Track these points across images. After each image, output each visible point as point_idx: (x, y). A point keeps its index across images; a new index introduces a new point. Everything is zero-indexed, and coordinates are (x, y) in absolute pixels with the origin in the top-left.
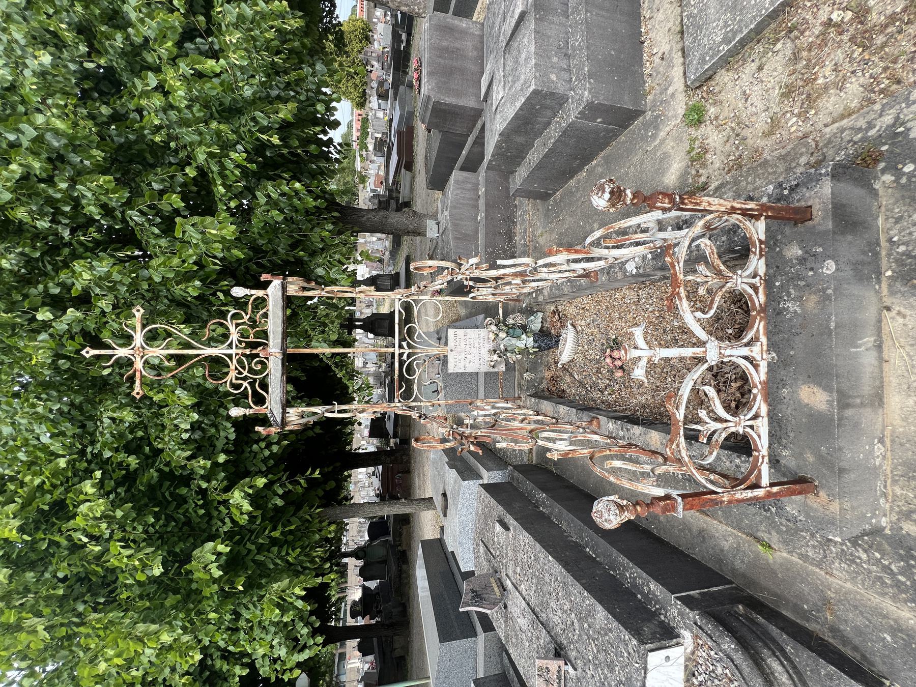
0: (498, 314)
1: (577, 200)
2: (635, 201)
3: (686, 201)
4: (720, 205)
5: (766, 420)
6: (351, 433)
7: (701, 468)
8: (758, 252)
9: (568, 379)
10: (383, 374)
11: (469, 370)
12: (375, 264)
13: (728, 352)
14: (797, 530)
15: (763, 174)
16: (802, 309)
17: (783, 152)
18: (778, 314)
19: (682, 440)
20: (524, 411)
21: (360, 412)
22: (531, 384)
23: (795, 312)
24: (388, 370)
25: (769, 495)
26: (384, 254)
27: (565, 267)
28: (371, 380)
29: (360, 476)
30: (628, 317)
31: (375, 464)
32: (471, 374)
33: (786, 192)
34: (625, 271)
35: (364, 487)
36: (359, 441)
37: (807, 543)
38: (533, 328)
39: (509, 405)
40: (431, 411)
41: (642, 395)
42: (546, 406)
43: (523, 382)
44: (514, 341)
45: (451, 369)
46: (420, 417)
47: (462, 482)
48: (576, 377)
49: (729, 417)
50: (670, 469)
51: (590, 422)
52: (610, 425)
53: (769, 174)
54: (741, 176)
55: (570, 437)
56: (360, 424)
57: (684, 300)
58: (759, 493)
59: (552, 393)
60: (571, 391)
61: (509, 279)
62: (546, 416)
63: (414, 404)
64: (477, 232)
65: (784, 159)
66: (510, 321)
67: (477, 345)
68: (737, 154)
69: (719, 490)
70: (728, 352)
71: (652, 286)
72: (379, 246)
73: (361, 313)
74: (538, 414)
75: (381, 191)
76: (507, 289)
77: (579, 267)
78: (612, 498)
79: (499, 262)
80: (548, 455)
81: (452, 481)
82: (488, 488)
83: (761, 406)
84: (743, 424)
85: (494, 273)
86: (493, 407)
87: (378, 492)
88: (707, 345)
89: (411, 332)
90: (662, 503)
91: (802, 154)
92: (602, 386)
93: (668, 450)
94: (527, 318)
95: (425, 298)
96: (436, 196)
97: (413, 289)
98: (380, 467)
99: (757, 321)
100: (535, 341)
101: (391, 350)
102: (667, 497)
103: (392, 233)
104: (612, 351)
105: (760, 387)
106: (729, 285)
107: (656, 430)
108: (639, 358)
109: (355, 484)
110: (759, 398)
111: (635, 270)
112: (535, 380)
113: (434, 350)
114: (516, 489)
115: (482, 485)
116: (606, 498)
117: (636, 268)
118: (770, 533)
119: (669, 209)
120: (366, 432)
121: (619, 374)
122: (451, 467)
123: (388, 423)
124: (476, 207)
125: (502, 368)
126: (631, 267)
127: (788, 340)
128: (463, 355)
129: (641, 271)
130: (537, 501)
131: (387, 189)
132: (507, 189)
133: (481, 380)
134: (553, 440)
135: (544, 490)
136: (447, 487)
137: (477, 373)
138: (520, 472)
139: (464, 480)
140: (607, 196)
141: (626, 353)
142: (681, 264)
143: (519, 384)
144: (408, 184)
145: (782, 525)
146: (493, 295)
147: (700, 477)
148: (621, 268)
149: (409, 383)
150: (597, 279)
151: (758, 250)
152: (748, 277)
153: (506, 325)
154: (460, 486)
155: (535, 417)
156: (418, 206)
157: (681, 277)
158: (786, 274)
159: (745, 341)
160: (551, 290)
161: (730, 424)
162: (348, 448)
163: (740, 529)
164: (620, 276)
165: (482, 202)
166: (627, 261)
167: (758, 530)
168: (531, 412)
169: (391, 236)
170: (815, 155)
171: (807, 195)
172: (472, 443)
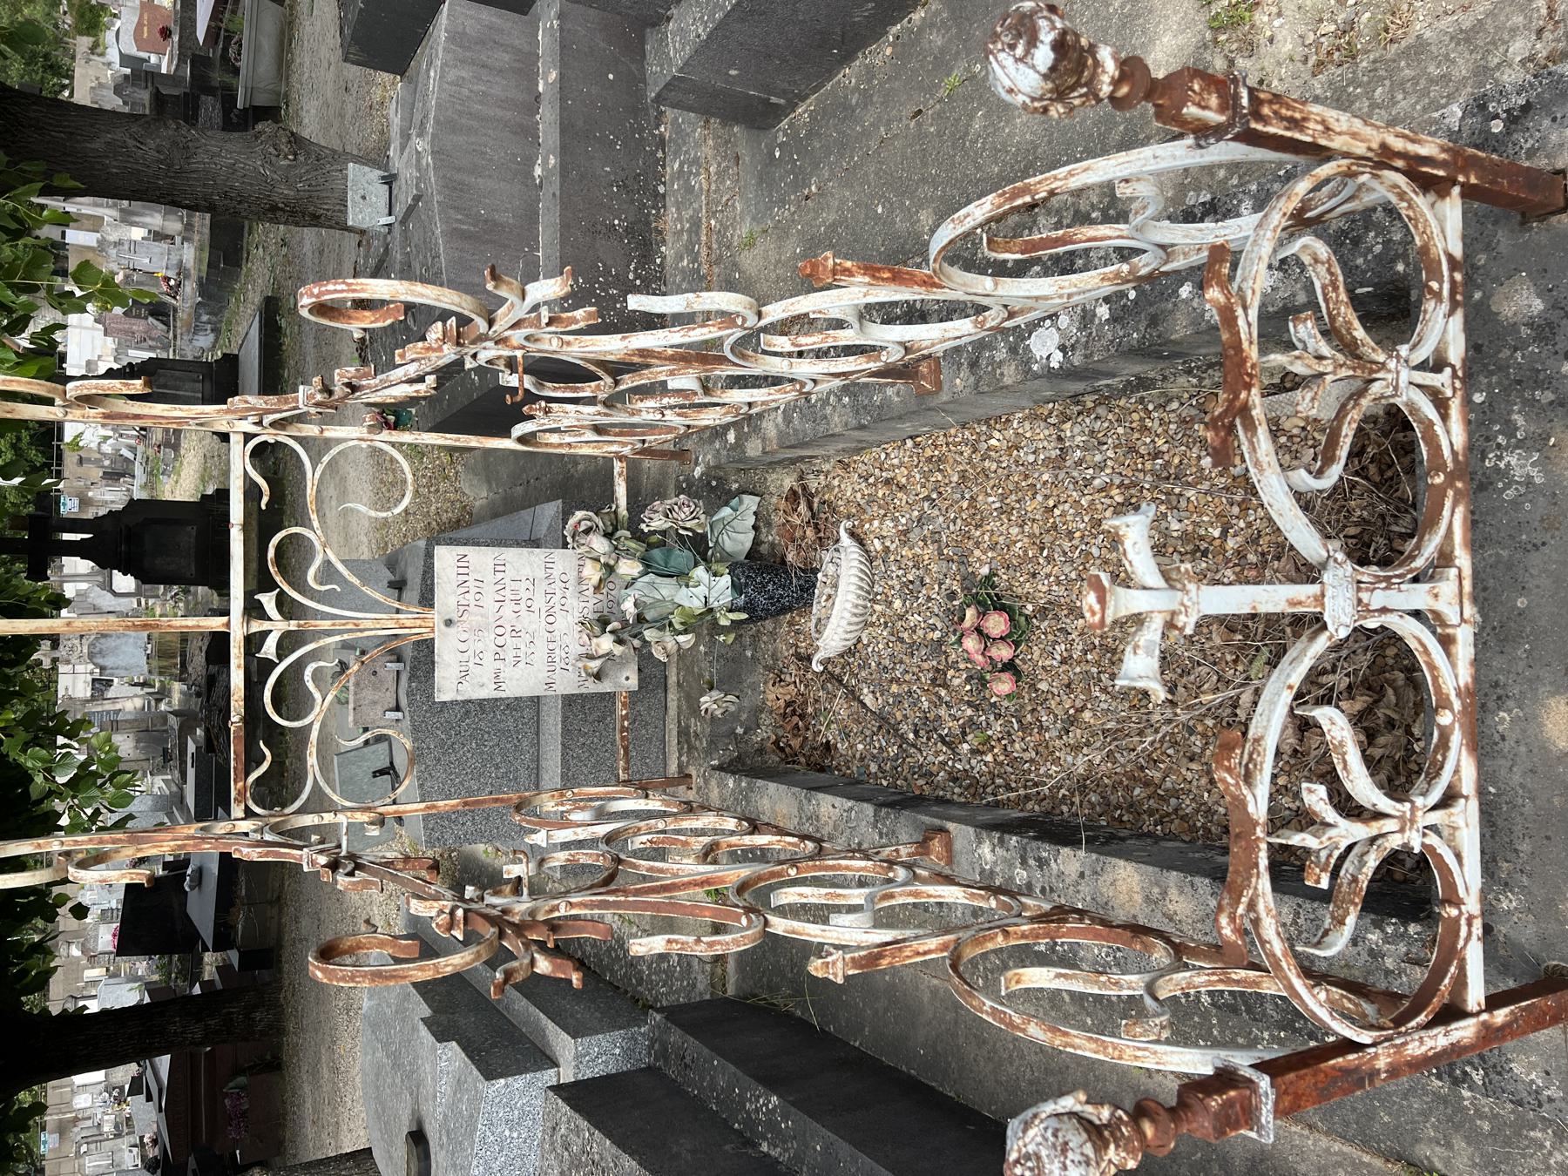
0: (610, 497)
1: (866, 134)
2: (1124, 90)
3: (1266, 110)
4: (1354, 135)
5: (1474, 804)
6: (42, 950)
7: (1314, 974)
8: (1446, 292)
9: (841, 708)
10: (173, 721)
11: (512, 690)
12: (139, 326)
13: (1377, 599)
14: (1522, 1125)
15: (1415, 80)
16: (1546, 472)
17: (1467, 21)
18: (1482, 487)
19: (1264, 884)
20: (706, 821)
21: (82, 865)
22: (721, 729)
23: (1529, 481)
24: (196, 704)
25: (1489, 1035)
26: (174, 291)
27: (846, 337)
28: (125, 745)
29: (82, 1101)
30: (1030, 506)
31: (141, 1052)
32: (515, 704)
33: (1497, 127)
34: (1026, 360)
35: (96, 1138)
36: (75, 968)
37: (1545, 1161)
38: (728, 545)
39: (654, 804)
40: (377, 842)
41: (1076, 748)
42: (776, 799)
43: (695, 726)
44: (667, 589)
45: (447, 686)
46: (334, 866)
47: (482, 1085)
48: (868, 700)
49: (1384, 804)
50: (1199, 980)
51: (923, 846)
52: (986, 850)
53: (1432, 81)
54: (1353, 82)
55: (871, 899)
56: (80, 911)
57: (1262, 432)
58: (1464, 1031)
59: (789, 756)
60: (854, 748)
61: (659, 372)
62: (782, 832)
63: (309, 820)
64: (532, 217)
65: (1467, 41)
66: (655, 522)
67: (539, 603)
68: (1340, 18)
69: (1365, 1037)
70: (1377, 599)
71: (1101, 411)
72: (156, 261)
73: (85, 502)
74: (755, 828)
75: (164, 63)
76: (647, 411)
77: (891, 335)
78: (1068, 1103)
79: (635, 302)
80: (815, 967)
81: (445, 1087)
82: (577, 1095)
83: (1460, 765)
84: (1421, 823)
85: (612, 346)
86: (602, 816)
87: (153, 1153)
88: (1327, 577)
89: (293, 557)
90: (1215, 1102)
91: (1514, 31)
92: (950, 726)
93: (1224, 920)
94: (709, 513)
95: (351, 434)
96: (377, 92)
97: (305, 396)
98: (164, 1062)
99: (1448, 504)
100: (736, 587)
101: (216, 623)
102: (1225, 1078)
103: (211, 208)
104: (982, 615)
105: (1457, 705)
106: (1376, 388)
107: (1128, 857)
108: (1138, 620)
109: (63, 1129)
110: (1456, 738)
111: (1058, 356)
112: (735, 717)
113: (377, 624)
114: (675, 1089)
115: (558, 1089)
116: (1049, 1108)
117: (1062, 348)
118: (1449, 1145)
119: (1218, 132)
120: (106, 938)
121: (1003, 685)
122: (442, 1035)
123: (193, 897)
124: (529, 133)
125: (627, 679)
126: (1045, 346)
127: (1510, 567)
128: (488, 642)
129: (1077, 359)
130: (750, 1123)
131: (188, 52)
132: (636, 81)
133: (552, 724)
134: (819, 914)
135: (772, 1083)
136: (426, 1109)
137: (536, 701)
138: (689, 1028)
139: (490, 1075)
140: (1044, 56)
141: (1102, 600)
142: (1253, 314)
143: (683, 733)
144: (268, 45)
145: (1482, 1116)
146: (598, 429)
147: (1316, 1002)
148: (1013, 350)
149: (287, 747)
150: (939, 385)
151: (1446, 286)
152: (1422, 366)
153: (639, 536)
154: (478, 1098)
155: (748, 840)
156: (310, 120)
157: (1253, 352)
158: (1502, 368)
159: (1419, 563)
160: (788, 420)
161: (1389, 825)
162: (30, 1001)
163: (1366, 1144)
164: (1010, 374)
165: (547, 119)
166: (1034, 326)
167: (1417, 1140)
168: (730, 824)
169: (202, 221)
170: (1547, 35)
171: (1554, 137)
172: (542, 946)
